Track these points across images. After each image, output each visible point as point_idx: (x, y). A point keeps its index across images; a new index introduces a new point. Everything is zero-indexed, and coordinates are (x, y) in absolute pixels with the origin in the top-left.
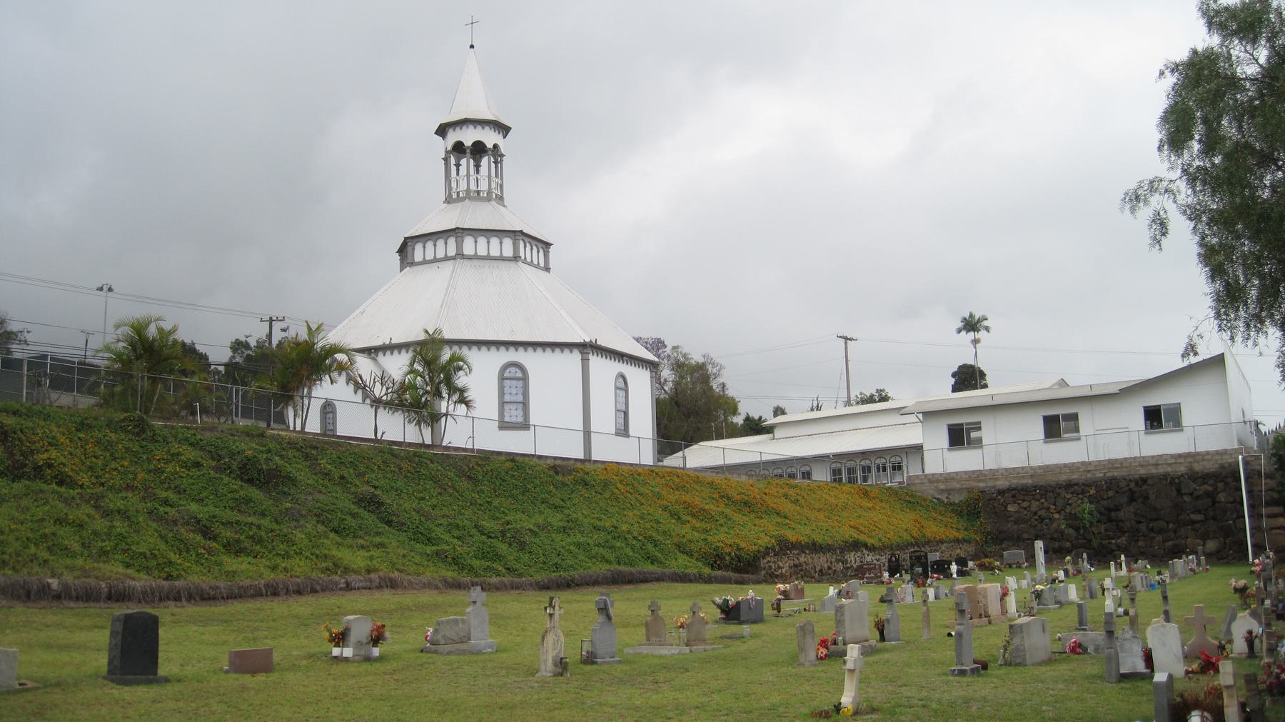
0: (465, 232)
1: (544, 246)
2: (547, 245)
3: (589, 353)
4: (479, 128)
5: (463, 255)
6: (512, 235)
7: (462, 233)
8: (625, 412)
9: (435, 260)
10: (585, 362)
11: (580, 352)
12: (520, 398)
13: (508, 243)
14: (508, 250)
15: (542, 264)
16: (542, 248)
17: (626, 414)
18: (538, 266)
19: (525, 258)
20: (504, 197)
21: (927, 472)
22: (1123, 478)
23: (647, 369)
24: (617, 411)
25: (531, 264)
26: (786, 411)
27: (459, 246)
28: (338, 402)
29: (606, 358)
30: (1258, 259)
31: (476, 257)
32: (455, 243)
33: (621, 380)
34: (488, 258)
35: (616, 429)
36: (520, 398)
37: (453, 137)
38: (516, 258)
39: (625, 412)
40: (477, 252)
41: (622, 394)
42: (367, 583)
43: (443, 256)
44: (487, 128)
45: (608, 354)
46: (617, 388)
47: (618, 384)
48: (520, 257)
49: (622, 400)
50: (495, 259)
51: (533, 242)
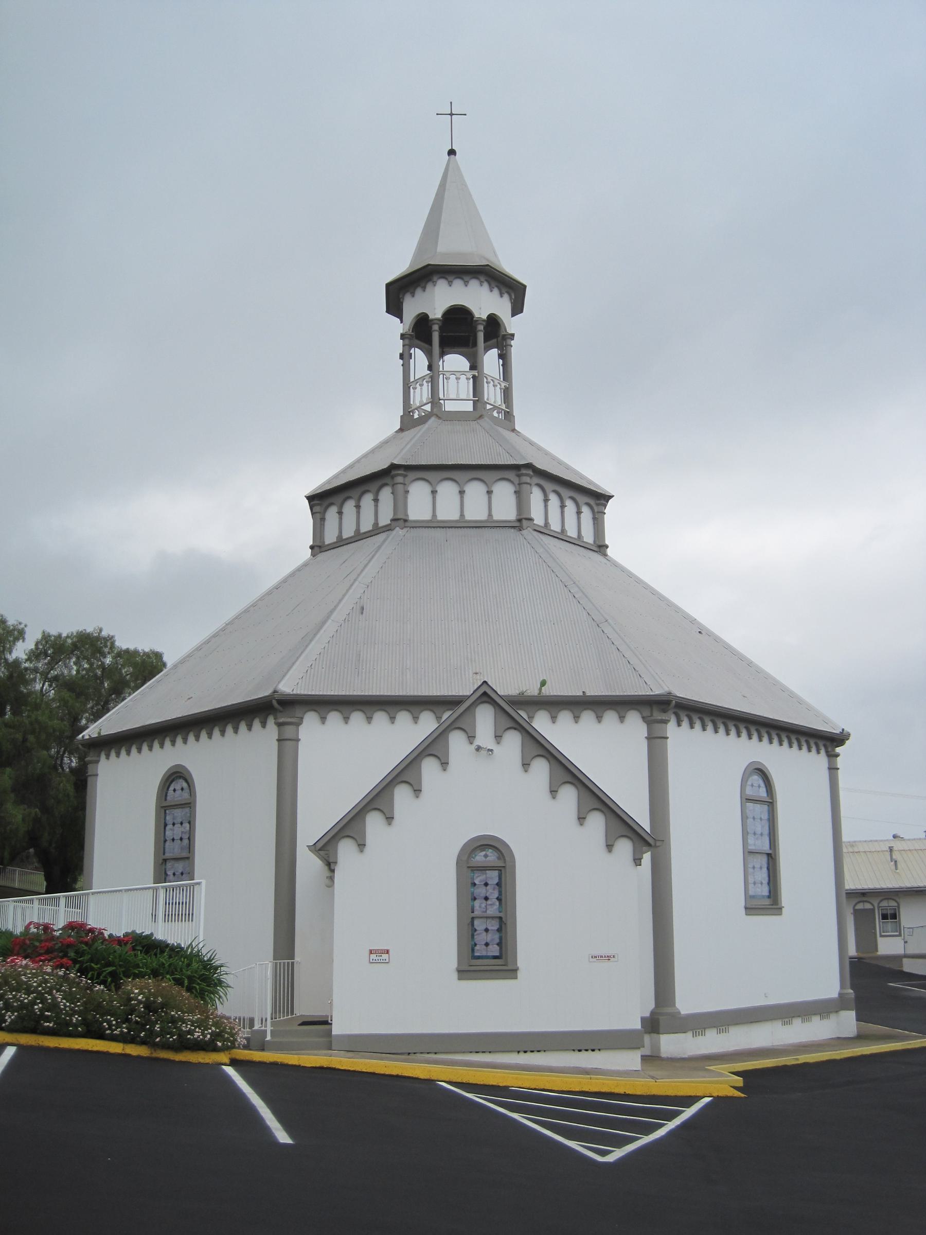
0: (412, 475)
1: (592, 502)
2: (599, 499)
3: (666, 722)
5: (406, 521)
6: (511, 475)
7: (405, 476)
8: (769, 855)
9: (359, 536)
12: (766, 847)
15: (588, 537)
16: (588, 504)
17: (772, 859)
18: (578, 543)
19: (547, 524)
20: (516, 413)
22: (282, 712)
23: (818, 752)
24: (749, 853)
25: (561, 536)
27: (400, 503)
29: (809, 750)
31: (434, 524)
33: (756, 779)
34: (462, 525)
35: (748, 897)
36: (766, 847)
37: (413, 307)
39: (769, 855)
41: (761, 811)
44: (474, 283)
45: (821, 744)
46: (746, 800)
47: (749, 791)
48: (531, 520)
49: (761, 827)
50: (477, 526)
51: (565, 493)
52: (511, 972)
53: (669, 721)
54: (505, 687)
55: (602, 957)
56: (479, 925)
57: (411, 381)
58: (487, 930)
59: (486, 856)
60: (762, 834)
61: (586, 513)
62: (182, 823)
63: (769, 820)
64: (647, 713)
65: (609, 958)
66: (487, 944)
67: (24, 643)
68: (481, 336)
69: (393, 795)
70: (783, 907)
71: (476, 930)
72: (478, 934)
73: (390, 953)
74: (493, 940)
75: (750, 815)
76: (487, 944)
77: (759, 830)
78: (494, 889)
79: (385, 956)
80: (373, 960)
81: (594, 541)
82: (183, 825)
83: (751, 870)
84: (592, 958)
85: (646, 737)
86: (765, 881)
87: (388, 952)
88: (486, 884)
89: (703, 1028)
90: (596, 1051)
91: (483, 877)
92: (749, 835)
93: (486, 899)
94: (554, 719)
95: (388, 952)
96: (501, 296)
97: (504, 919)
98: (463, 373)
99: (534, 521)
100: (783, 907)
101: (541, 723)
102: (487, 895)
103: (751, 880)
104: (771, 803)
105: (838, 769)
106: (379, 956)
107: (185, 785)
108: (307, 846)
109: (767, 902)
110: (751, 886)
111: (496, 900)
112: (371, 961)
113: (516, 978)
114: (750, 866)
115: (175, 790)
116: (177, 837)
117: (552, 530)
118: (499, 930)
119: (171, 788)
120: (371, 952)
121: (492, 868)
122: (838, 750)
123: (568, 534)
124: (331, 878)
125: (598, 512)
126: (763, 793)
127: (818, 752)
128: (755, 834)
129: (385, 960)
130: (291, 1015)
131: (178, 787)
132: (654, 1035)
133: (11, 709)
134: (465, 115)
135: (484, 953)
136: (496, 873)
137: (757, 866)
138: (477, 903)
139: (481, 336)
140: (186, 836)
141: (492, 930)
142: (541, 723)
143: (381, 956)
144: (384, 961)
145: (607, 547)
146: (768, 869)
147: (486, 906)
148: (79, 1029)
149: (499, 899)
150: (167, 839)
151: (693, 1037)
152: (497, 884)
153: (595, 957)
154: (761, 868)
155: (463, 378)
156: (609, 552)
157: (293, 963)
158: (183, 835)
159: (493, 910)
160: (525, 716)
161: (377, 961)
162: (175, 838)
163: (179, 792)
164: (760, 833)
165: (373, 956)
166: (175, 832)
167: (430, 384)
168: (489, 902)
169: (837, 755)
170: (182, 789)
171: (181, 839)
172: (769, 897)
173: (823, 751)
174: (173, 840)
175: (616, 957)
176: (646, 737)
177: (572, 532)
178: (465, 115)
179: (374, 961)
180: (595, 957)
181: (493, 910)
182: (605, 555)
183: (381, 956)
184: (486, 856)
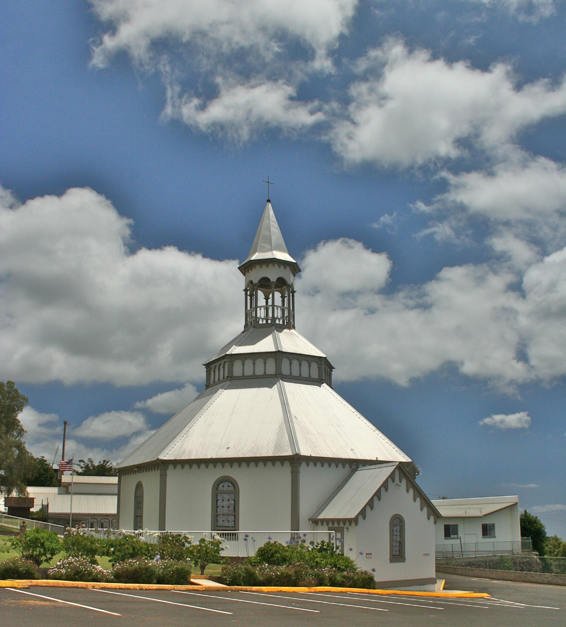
43: (263, 374)
57: (248, 310)
67: (45, 456)
78: (398, 532)
79: (371, 556)
93: (397, 535)
95: (371, 554)
97: (401, 543)
98: (280, 307)
105: (205, 385)
113: (405, 562)
117: (303, 377)
120: (367, 554)
124: (194, 401)
133: (189, 560)
134: (42, 500)
138: (394, 537)
149: (400, 536)
155: (279, 308)
165: (368, 556)
167: (265, 310)
168: (397, 537)
178: (42, 500)
181: (398, 539)
184: (396, 521)
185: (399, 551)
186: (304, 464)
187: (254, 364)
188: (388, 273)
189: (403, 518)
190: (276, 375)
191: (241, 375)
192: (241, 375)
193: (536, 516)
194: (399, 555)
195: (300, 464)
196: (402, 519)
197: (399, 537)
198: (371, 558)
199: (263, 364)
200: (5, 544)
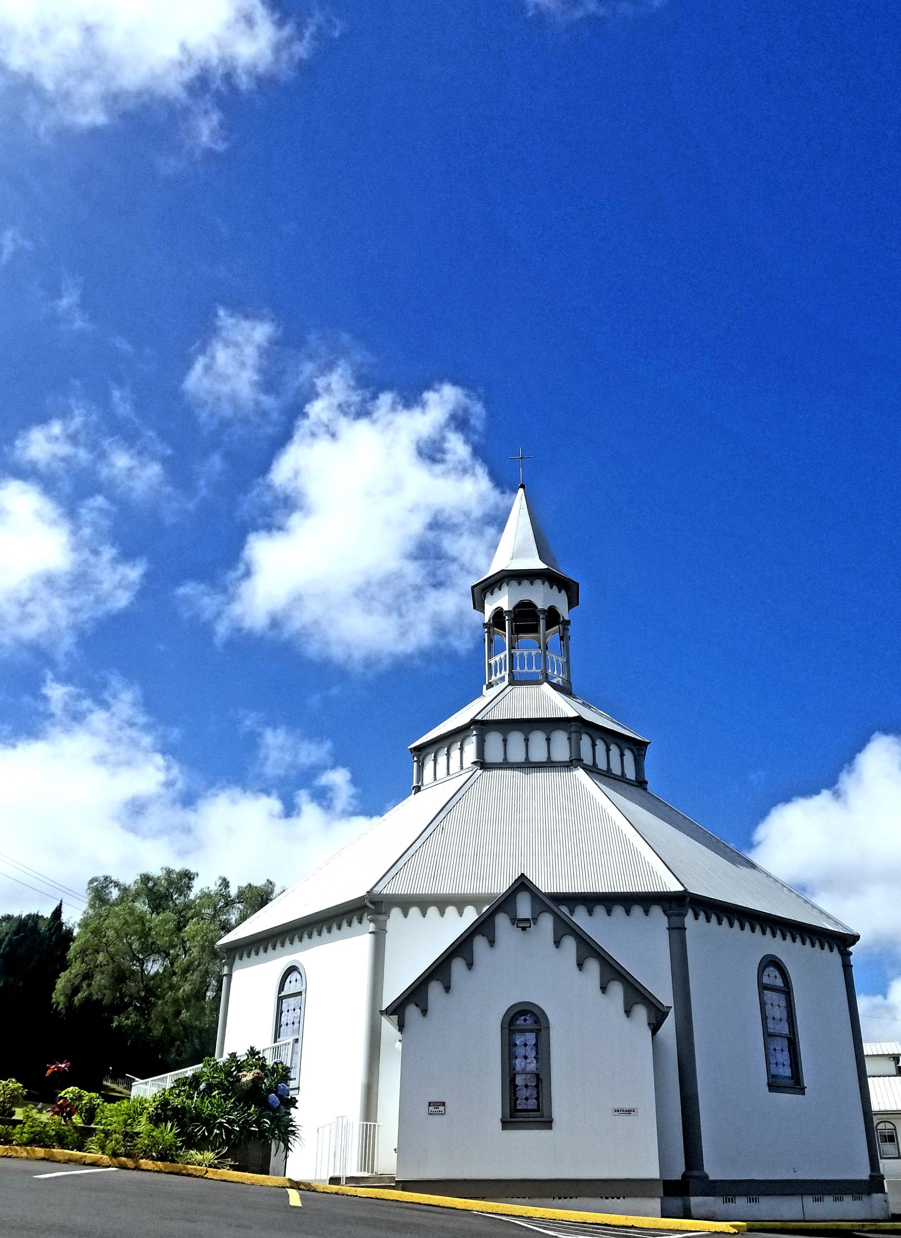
4: (526, 583)
10: (677, 932)
11: (665, 912)
13: (560, 739)
14: (561, 751)
15: (631, 774)
21: (868, 1079)
24: (768, 1036)
26: (259, 882)
28: (891, 1128)
30: (65, 715)
32: (566, 743)
33: (772, 971)
36: (785, 1030)
38: (575, 762)
39: (789, 1040)
40: (552, 755)
41: (775, 999)
42: (105, 1156)
43: (523, 760)
44: (538, 582)
46: (763, 987)
47: (766, 980)
49: (778, 1011)
52: (547, 1124)
53: (686, 915)
54: (545, 885)
55: (623, 1111)
56: (519, 1080)
58: (526, 1086)
59: (525, 1020)
60: (781, 1020)
61: (629, 756)
62: (294, 1010)
63: (787, 1007)
64: (667, 906)
65: (629, 1112)
66: (527, 1099)
68: (542, 623)
69: (450, 969)
70: (806, 1087)
71: (517, 1086)
72: (520, 1090)
73: (446, 1105)
74: (532, 1095)
75: (769, 1002)
76: (527, 1099)
77: (778, 1016)
79: (441, 1108)
80: (431, 1111)
81: (636, 778)
82: (295, 1011)
83: (772, 1051)
84: (615, 1112)
85: (667, 928)
86: (788, 1063)
87: (444, 1104)
88: (525, 1045)
89: (733, 1195)
90: (419, 1008)
91: (523, 1039)
92: (768, 1019)
93: (526, 1057)
94: (590, 912)
95: (444, 1104)
96: (560, 592)
99: (583, 761)
100: (806, 1087)
101: (580, 918)
102: (527, 1054)
103: (773, 1061)
104: (787, 991)
106: (436, 1108)
107: (299, 977)
108: (380, 1011)
109: (790, 1083)
110: (773, 1066)
111: (534, 1059)
112: (430, 1112)
114: (772, 1047)
115: (290, 982)
116: (290, 1022)
118: (537, 1086)
119: (288, 980)
120: (430, 1104)
121: (531, 1031)
122: (851, 949)
123: (627, 777)
125: (638, 755)
126: (779, 982)
127: (831, 950)
128: (774, 1019)
129: (442, 1111)
130: (371, 1173)
131: (293, 979)
132: (686, 1198)
135: (525, 1107)
136: (534, 1035)
137: (779, 1048)
139: (542, 623)
140: (296, 1021)
141: (531, 1086)
142: (580, 918)
143: (438, 1108)
144: (440, 1113)
145: (646, 783)
146: (789, 1051)
147: (525, 1064)
148: (58, 967)
150: (282, 1024)
151: (724, 1203)
152: (534, 1045)
153: (618, 1111)
154: (782, 1050)
156: (648, 786)
157: (375, 1126)
158: (295, 1019)
159: (532, 1066)
160: (567, 913)
161: (435, 1113)
162: (288, 1023)
163: (294, 983)
164: (779, 1018)
165: (432, 1108)
166: (289, 1018)
168: (528, 1061)
169: (851, 953)
170: (296, 980)
171: (293, 1023)
172: (792, 1078)
173: (836, 950)
174: (287, 1024)
175: (636, 1110)
176: (667, 928)
177: (616, 770)
179: (432, 1113)
180: (618, 1111)
181: (532, 1066)
182: (645, 789)
183: (438, 1108)
184: (525, 1020)
185: (537, 1099)
186: (396, 912)
187: (527, 740)
188: (14, 746)
189: (520, 1003)
190: (571, 761)
191: (524, 761)
192: (524, 761)
193: (217, 877)
194: (538, 1110)
195: (387, 914)
196: (522, 1008)
197: (535, 1061)
198: (443, 1114)
199: (523, 744)
200: (406, 121)
